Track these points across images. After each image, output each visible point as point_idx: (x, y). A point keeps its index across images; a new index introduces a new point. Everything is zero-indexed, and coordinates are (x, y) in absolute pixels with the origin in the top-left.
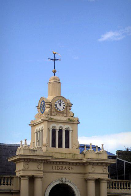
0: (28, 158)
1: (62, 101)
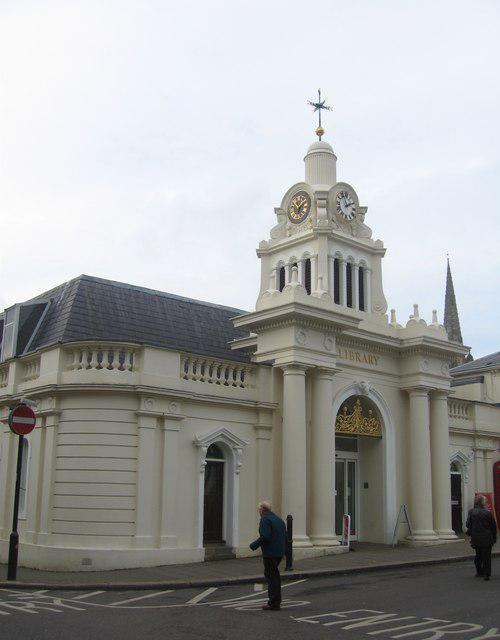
0: (325, 317)
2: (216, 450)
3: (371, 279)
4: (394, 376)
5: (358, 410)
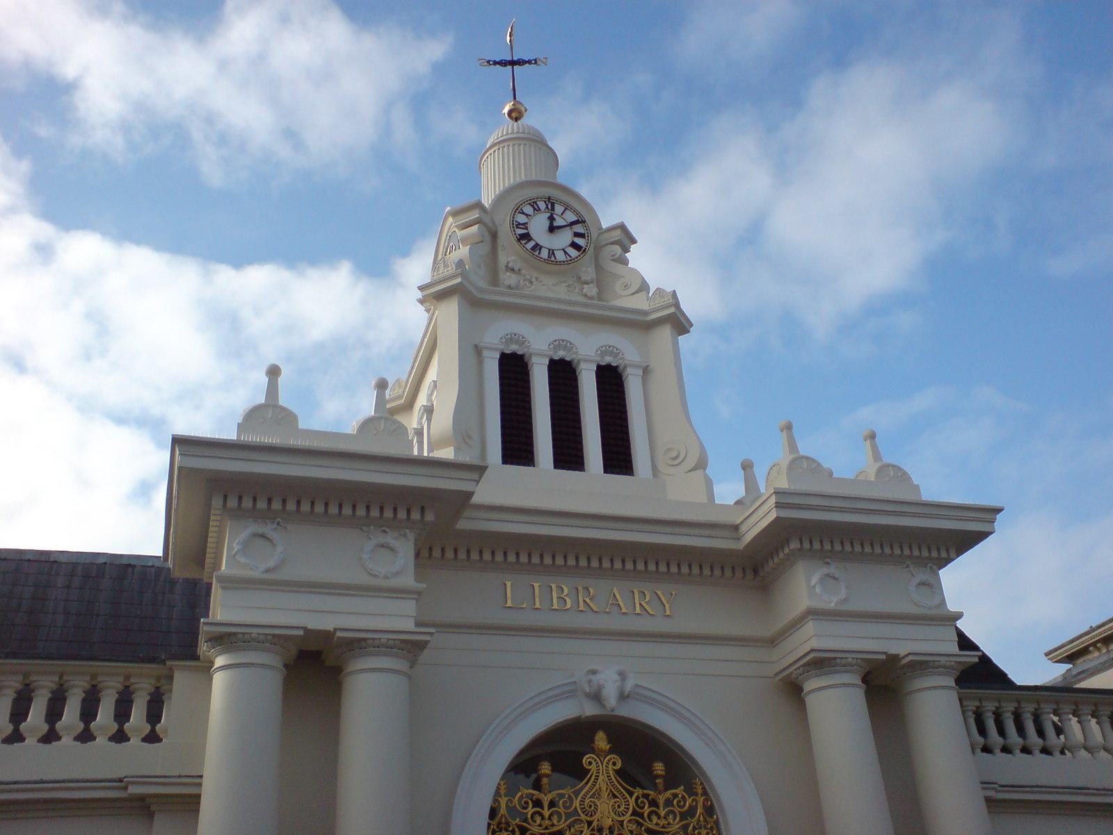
1: (559, 209)
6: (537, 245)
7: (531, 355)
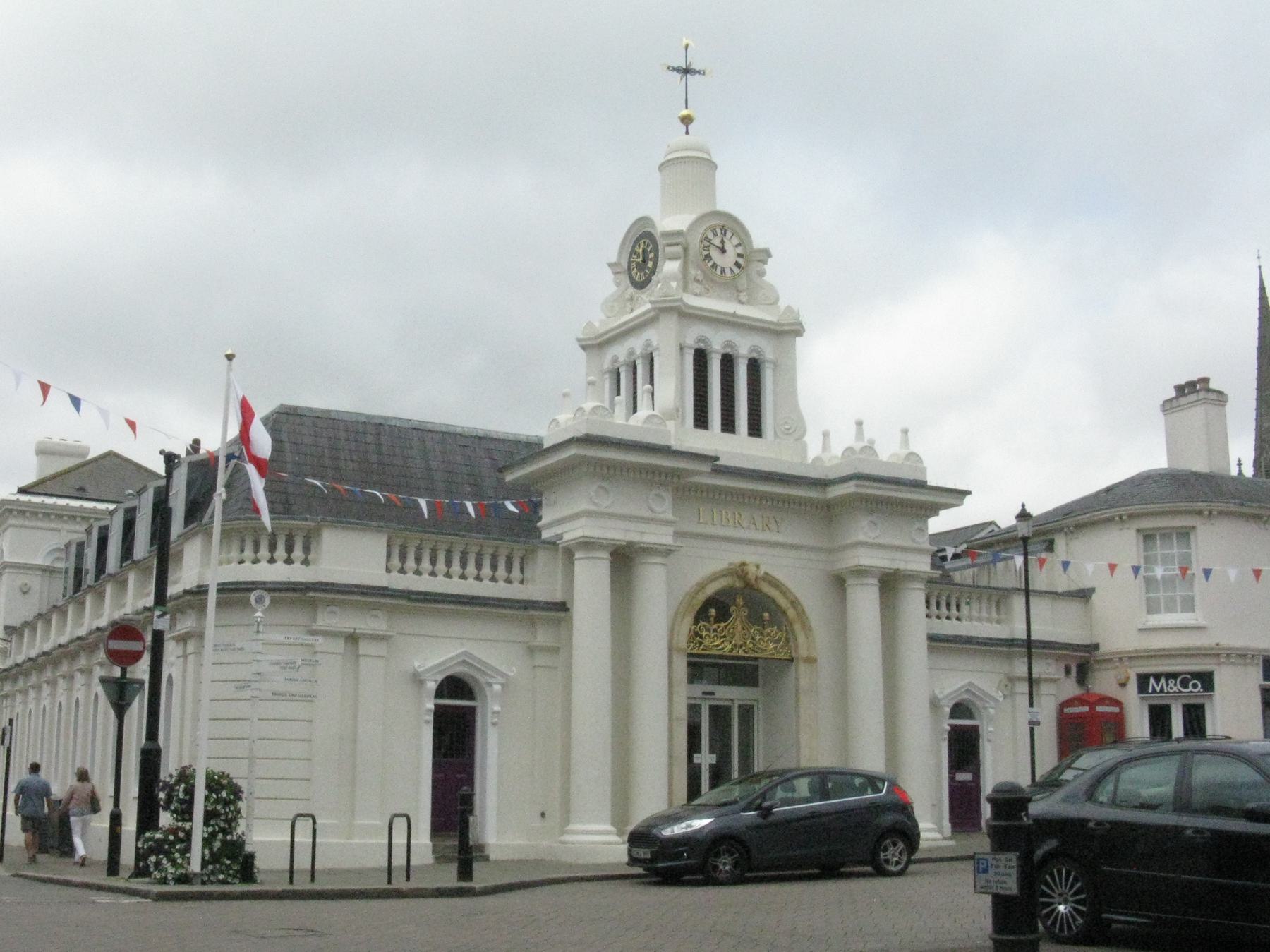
1: (729, 234)
2: (455, 686)
3: (775, 383)
4: (821, 550)
5: (738, 613)
6: (715, 263)
7: (712, 352)
